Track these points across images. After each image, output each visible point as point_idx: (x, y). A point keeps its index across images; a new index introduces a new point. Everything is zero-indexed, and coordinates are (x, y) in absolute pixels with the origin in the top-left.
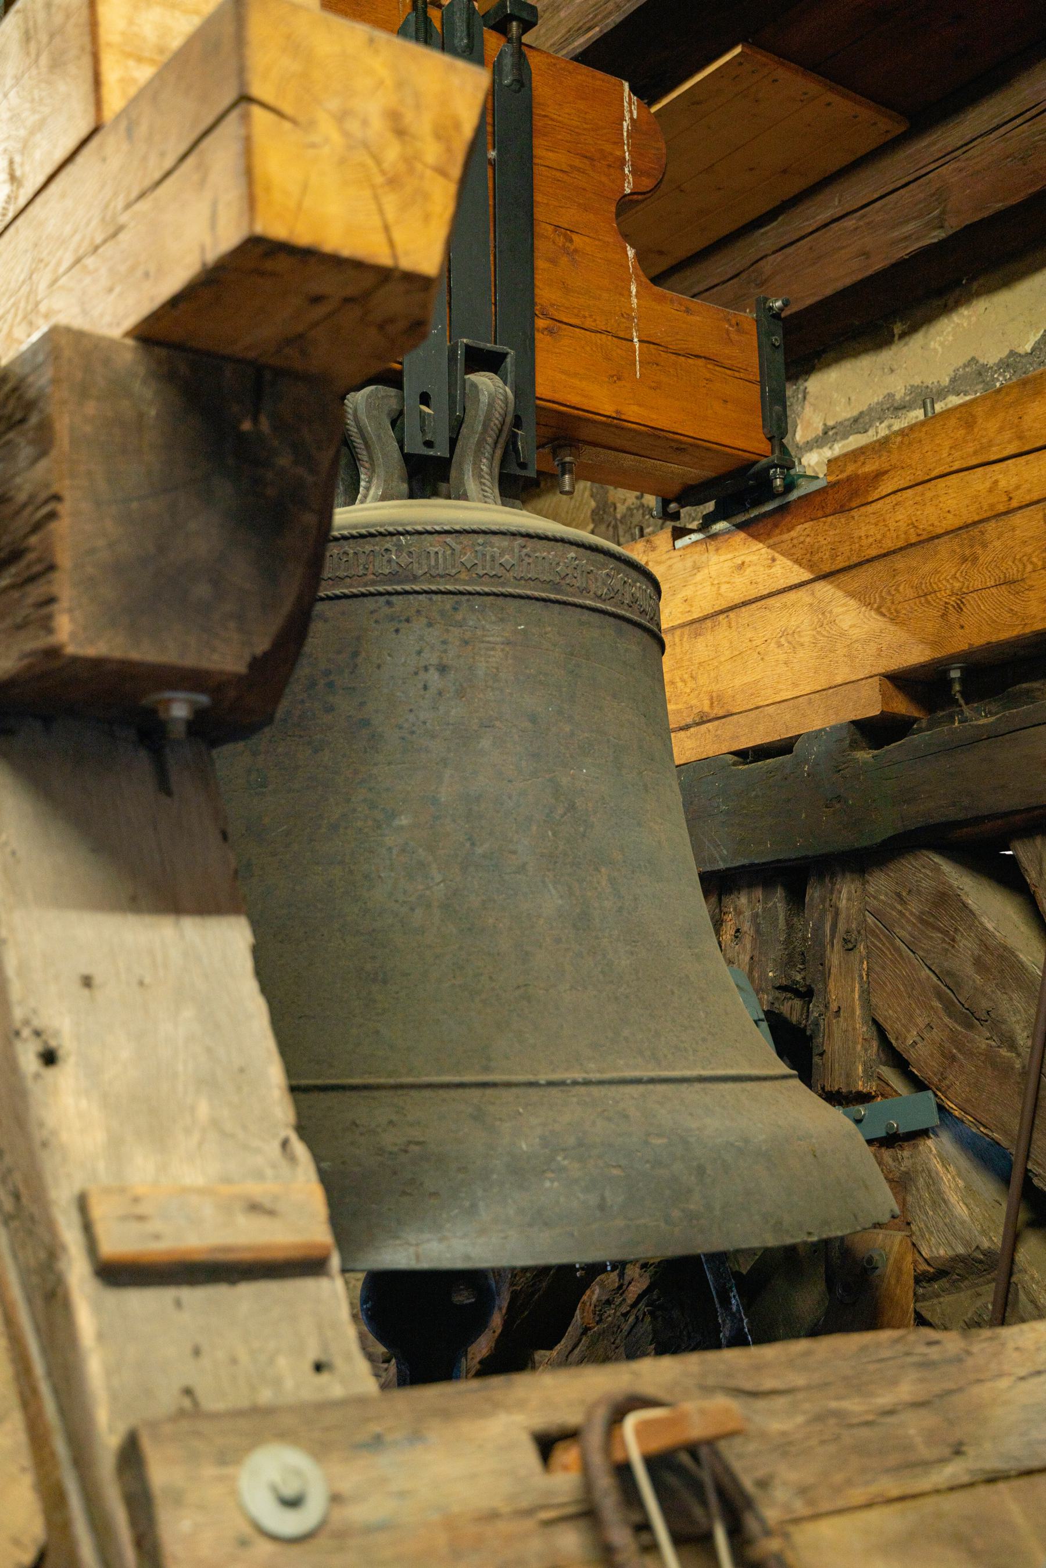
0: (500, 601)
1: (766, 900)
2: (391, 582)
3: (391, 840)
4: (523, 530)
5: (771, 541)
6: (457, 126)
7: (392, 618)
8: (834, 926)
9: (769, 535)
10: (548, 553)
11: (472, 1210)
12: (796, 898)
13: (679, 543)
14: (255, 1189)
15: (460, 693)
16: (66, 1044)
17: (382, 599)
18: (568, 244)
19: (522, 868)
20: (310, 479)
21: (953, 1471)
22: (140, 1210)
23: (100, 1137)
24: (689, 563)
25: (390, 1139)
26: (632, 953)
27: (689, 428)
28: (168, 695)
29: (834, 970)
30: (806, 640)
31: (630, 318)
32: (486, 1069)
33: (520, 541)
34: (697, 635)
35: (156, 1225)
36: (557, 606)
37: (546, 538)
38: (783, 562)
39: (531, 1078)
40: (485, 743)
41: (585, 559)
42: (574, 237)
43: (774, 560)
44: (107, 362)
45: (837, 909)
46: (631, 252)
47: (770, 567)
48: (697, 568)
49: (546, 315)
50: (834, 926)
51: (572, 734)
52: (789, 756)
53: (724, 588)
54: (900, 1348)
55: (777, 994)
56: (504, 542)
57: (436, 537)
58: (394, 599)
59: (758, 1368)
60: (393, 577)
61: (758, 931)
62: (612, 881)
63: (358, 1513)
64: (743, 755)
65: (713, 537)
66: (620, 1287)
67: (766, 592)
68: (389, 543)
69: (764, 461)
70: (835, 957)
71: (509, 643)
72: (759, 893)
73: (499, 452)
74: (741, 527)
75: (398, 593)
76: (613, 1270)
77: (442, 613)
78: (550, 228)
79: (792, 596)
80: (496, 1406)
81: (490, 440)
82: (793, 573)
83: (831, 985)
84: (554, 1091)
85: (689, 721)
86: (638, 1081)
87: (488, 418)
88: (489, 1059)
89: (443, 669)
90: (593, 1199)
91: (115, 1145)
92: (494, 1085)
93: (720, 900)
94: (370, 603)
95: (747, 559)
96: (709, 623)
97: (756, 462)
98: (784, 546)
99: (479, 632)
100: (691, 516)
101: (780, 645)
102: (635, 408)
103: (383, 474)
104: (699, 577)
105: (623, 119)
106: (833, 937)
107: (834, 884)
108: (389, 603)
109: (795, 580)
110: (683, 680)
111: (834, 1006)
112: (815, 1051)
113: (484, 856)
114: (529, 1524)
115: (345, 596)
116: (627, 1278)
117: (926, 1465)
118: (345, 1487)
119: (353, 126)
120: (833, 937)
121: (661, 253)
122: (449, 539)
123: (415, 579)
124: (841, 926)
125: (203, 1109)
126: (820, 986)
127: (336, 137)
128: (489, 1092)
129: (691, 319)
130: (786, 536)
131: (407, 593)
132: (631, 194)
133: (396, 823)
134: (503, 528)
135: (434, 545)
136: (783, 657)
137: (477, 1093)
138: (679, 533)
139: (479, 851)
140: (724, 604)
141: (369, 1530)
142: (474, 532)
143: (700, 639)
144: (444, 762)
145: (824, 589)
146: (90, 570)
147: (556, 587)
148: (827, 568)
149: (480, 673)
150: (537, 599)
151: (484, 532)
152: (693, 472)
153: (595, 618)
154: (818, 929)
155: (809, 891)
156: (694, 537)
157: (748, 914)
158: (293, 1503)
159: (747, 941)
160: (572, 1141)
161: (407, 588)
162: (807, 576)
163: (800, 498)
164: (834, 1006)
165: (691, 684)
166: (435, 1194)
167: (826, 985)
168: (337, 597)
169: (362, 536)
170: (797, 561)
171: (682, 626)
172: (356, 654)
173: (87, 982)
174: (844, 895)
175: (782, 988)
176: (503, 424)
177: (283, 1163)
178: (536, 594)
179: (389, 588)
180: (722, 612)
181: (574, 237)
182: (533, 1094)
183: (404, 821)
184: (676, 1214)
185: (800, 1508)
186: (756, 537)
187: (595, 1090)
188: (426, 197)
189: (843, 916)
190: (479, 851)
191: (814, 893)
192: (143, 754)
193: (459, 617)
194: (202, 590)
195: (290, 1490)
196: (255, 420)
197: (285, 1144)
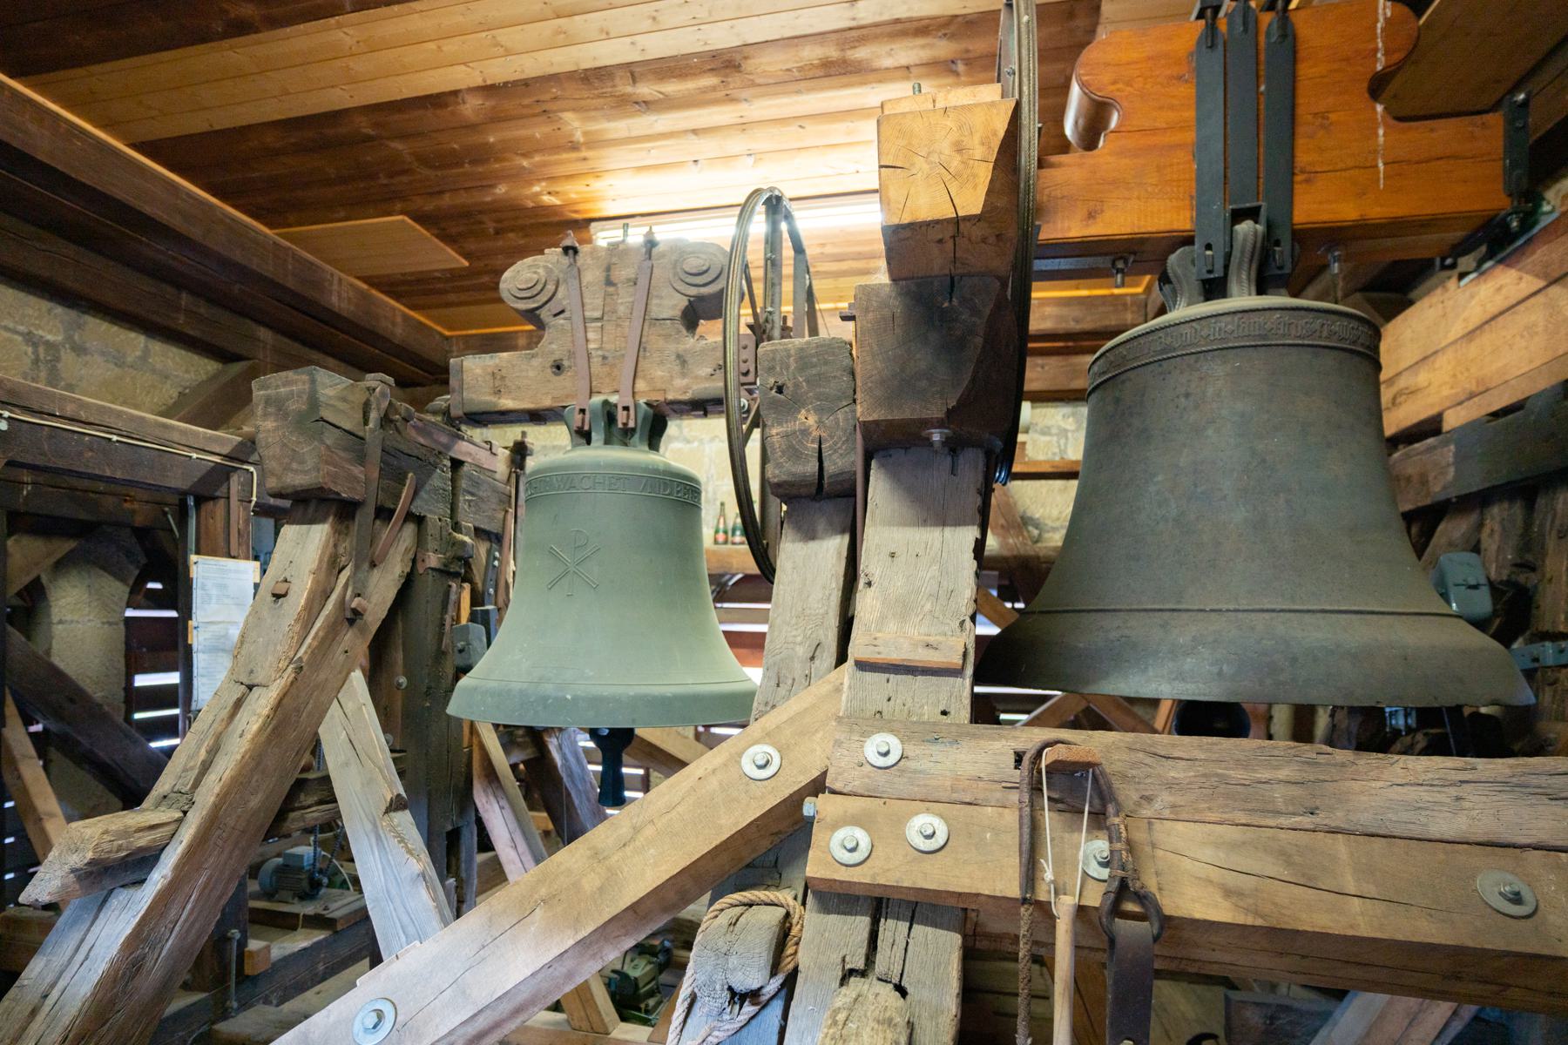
0: (1225, 352)
1: (1510, 508)
2: (1162, 354)
3: (1152, 489)
4: (1240, 309)
5: (1519, 267)
6: (995, 134)
7: (1161, 373)
8: (1553, 522)
9: (1518, 262)
10: (1255, 317)
11: (1145, 671)
12: (1530, 506)
13: (1463, 282)
14: (931, 640)
15: (1197, 407)
16: (875, 579)
17: (1156, 364)
18: (1325, 122)
19: (1224, 498)
20: (979, 321)
21: (1307, 821)
22: (875, 642)
23: (876, 614)
24: (1468, 294)
25: (1113, 635)
26: (1294, 541)
27: (1428, 209)
28: (933, 431)
29: (1550, 552)
30: (1540, 329)
31: (1376, 152)
32: (1179, 602)
33: (1240, 315)
34: (1471, 341)
35: (881, 649)
36: (1264, 348)
37: (1257, 310)
38: (1528, 278)
39: (1202, 607)
40: (1210, 432)
41: (1287, 317)
42: (1330, 115)
43: (1521, 278)
44: (877, 295)
45: (1555, 510)
46: (1379, 108)
47: (1518, 284)
48: (1472, 297)
49: (1303, 172)
50: (1553, 522)
51: (1269, 420)
52: (1522, 412)
53: (1489, 306)
54: (1293, 752)
55: (1514, 569)
56: (1228, 318)
57: (1187, 325)
58: (1163, 363)
59: (1174, 746)
60: (1163, 351)
61: (1504, 529)
62: (1287, 501)
63: (912, 765)
64: (1495, 415)
65: (1482, 274)
66: (1412, 745)
67: (1514, 302)
68: (1161, 334)
69: (1503, 213)
70: (1551, 543)
71: (1227, 375)
72: (1506, 505)
73: (1254, 266)
74: (1500, 262)
75: (1164, 359)
76: (1407, 734)
77: (1189, 366)
78: (1310, 117)
79: (1532, 300)
80: (1001, 737)
81: (1246, 260)
82: (1530, 283)
83: (1547, 562)
84: (1213, 614)
85: (1463, 398)
86: (1273, 611)
87: (1243, 247)
88: (1182, 597)
89: (1187, 395)
90: (1215, 670)
91: (883, 619)
92: (1180, 610)
93: (1482, 513)
94: (1151, 368)
95: (1502, 282)
96: (1478, 332)
97: (1496, 215)
98: (1529, 267)
99: (1210, 372)
100: (1466, 262)
101: (1522, 336)
102: (1379, 209)
103: (1187, 295)
104: (1473, 302)
105: (1377, 21)
106: (1551, 529)
107: (1554, 494)
108: (1160, 365)
109: (1535, 289)
110: (1462, 373)
111: (1548, 576)
112: (1534, 605)
113: (1202, 493)
114: (999, 786)
115: (1139, 366)
116: (1416, 740)
117: (1278, 813)
118: (908, 753)
119: (935, 158)
120: (1551, 529)
121: (1498, 81)
122: (1194, 324)
123: (1175, 349)
124: (1557, 522)
125: (928, 606)
126: (1541, 563)
127: (926, 167)
128: (1175, 614)
129: (1434, 135)
130: (1529, 260)
131: (1169, 358)
132: (1383, 69)
133: (1155, 480)
134: (1227, 311)
135: (1185, 329)
136: (1524, 344)
137: (1168, 614)
138: (1462, 276)
139: (1199, 490)
140: (1488, 316)
141: (915, 772)
142: (1208, 317)
143: (1473, 343)
144: (1184, 445)
145: (1555, 290)
146: (870, 385)
147: (1264, 337)
148: (1557, 275)
149: (1209, 394)
150: (1248, 346)
151: (1215, 316)
152: (1457, 235)
153: (1293, 349)
154: (1542, 525)
155: (1538, 500)
156: (1472, 276)
157: (1498, 519)
158: (886, 754)
159: (1496, 537)
160: (1210, 639)
161: (1169, 355)
162: (1542, 284)
163: (1540, 230)
164: (1548, 576)
165: (1466, 374)
166: (1128, 661)
167: (1544, 561)
168: (1135, 368)
169: (1148, 333)
170: (1537, 276)
171: (1462, 337)
172: (1143, 395)
173: (893, 555)
174: (1561, 500)
175: (1516, 565)
176: (1254, 247)
177: (959, 630)
178: (1248, 344)
179: (1160, 358)
180: (1487, 322)
181: (1330, 115)
182: (1200, 615)
183: (1160, 478)
184: (1268, 681)
185: (1167, 813)
186: (1509, 266)
187: (1240, 615)
188: (975, 176)
189: (1559, 516)
190: (1199, 490)
191: (1541, 502)
192: (949, 459)
193: (1198, 365)
194: (924, 383)
195: (884, 750)
196: (951, 301)
197: (962, 623)
